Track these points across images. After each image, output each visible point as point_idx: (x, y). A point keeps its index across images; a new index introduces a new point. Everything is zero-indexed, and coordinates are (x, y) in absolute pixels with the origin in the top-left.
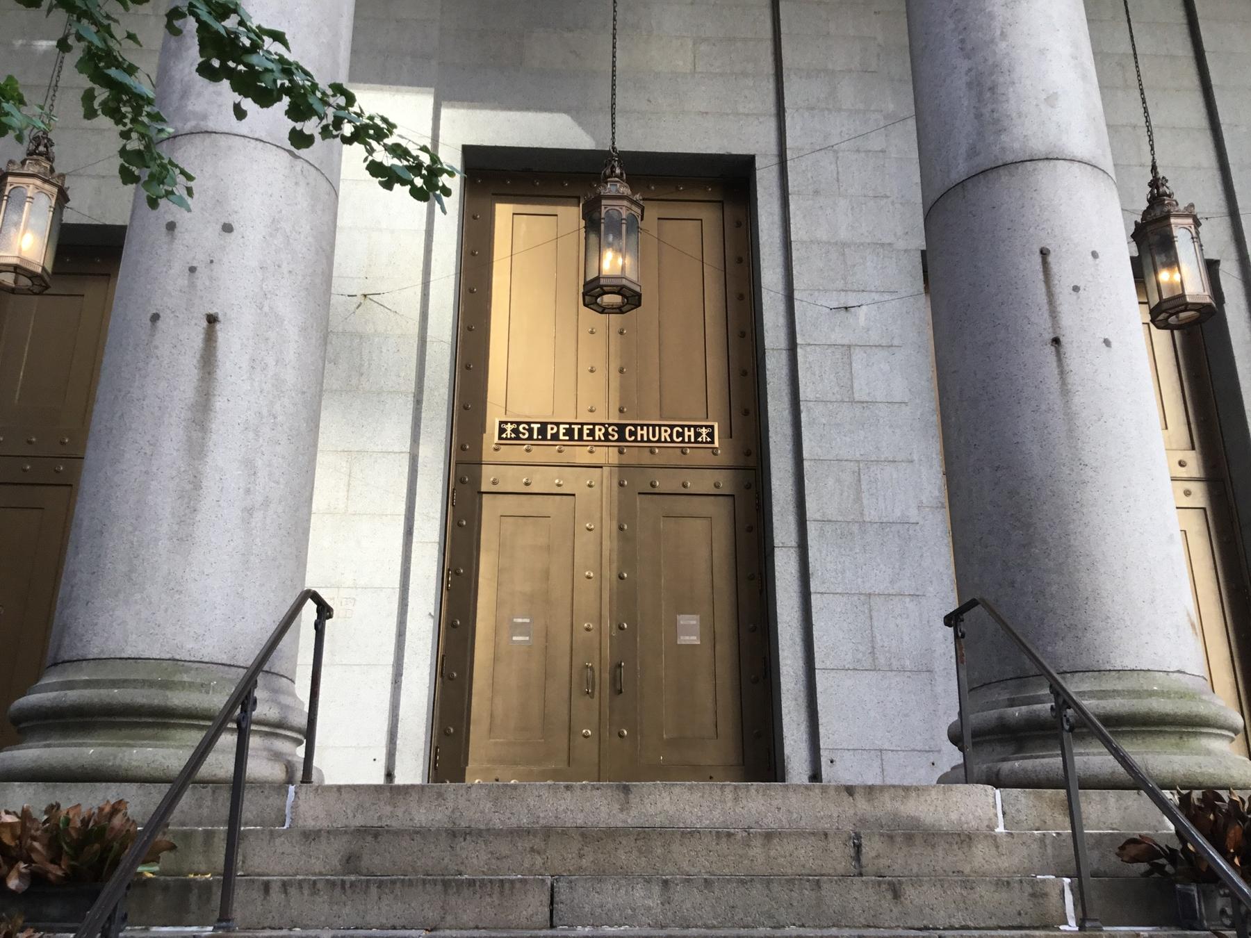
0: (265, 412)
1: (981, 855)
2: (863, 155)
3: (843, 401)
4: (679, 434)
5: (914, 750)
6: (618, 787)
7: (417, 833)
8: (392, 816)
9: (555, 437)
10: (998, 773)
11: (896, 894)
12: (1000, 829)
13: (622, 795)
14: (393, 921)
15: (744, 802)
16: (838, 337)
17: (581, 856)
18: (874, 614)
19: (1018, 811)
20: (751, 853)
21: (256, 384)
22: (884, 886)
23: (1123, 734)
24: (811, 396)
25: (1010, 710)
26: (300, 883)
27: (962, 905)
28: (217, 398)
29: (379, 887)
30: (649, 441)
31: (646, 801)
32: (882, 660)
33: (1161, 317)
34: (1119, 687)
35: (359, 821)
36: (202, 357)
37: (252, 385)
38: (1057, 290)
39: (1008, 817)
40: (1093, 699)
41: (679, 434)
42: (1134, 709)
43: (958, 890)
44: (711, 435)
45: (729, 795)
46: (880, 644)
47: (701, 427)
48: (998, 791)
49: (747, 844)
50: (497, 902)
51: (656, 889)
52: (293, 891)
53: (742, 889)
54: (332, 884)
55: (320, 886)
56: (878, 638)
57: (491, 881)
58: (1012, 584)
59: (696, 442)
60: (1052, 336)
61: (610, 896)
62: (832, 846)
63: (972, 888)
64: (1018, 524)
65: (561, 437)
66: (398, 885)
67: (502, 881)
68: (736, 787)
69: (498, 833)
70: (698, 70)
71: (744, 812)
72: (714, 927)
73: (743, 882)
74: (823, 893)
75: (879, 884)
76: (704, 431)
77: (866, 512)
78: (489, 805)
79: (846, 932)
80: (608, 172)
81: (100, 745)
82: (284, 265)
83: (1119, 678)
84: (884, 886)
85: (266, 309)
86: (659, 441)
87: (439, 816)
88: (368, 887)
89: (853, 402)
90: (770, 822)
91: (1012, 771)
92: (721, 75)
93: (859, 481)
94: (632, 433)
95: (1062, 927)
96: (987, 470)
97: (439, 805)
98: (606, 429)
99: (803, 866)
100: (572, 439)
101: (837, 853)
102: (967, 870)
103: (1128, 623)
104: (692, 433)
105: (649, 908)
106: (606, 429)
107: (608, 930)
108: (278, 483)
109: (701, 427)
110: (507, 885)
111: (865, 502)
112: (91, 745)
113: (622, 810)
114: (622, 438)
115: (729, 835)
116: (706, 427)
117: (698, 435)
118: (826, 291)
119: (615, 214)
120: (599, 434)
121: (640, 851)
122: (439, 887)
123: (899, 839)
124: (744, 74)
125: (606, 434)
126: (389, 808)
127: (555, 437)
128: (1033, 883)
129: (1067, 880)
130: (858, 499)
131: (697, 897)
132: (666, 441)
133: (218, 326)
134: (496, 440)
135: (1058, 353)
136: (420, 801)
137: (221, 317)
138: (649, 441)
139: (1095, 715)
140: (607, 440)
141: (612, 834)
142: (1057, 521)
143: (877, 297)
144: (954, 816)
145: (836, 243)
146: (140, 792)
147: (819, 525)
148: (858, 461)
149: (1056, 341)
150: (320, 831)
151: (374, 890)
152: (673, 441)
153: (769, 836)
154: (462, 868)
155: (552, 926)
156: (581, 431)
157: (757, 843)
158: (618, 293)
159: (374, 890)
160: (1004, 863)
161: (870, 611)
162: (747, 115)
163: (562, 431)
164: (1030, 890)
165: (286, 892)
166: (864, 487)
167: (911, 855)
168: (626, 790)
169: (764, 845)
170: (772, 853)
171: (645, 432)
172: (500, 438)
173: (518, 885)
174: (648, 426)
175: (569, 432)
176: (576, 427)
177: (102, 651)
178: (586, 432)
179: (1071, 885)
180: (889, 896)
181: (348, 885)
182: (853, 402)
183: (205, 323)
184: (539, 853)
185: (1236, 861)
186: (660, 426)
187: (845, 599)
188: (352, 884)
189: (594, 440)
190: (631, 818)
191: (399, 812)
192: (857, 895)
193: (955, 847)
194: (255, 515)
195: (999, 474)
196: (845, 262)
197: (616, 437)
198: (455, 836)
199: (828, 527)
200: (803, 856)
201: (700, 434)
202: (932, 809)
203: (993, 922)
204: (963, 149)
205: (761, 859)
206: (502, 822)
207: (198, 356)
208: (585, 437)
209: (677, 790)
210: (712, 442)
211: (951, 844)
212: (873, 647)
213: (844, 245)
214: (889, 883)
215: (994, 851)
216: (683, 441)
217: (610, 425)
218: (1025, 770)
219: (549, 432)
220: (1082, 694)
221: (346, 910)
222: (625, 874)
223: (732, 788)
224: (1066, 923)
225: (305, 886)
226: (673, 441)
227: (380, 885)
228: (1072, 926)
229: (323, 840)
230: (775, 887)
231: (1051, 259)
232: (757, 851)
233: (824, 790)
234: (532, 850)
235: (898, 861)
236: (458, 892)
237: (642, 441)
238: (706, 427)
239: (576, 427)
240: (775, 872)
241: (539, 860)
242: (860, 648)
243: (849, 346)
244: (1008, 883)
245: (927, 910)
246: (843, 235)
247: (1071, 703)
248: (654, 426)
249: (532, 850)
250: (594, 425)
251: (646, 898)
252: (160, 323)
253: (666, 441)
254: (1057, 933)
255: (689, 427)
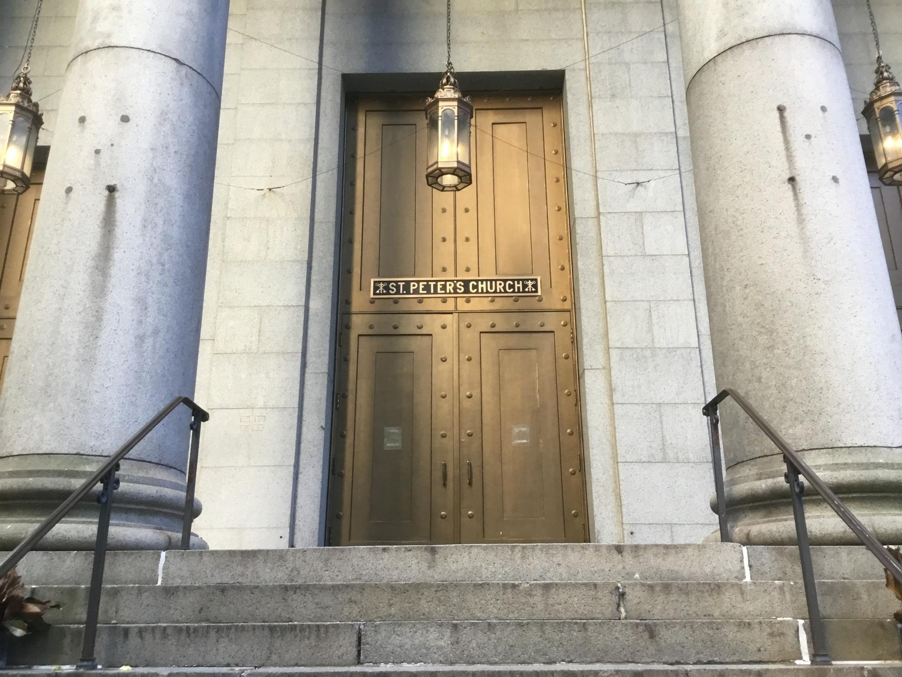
0: (154, 260)
1: (728, 601)
2: (649, 66)
3: (636, 255)
4: (510, 286)
5: (697, 524)
6: (426, 549)
7: (257, 587)
8: (242, 575)
9: (416, 291)
10: (748, 535)
11: (652, 636)
12: (748, 579)
13: (429, 554)
14: (229, 660)
15: (531, 559)
16: (632, 206)
17: (390, 605)
18: (664, 418)
19: (763, 564)
20: (531, 601)
21: (148, 239)
22: (641, 628)
23: (853, 499)
24: (611, 253)
25: (758, 483)
26: (153, 629)
27: (709, 643)
28: (116, 250)
29: (217, 632)
30: (487, 292)
31: (449, 560)
32: (671, 455)
33: (887, 175)
34: (850, 461)
35: (217, 580)
36: (104, 219)
37: (144, 240)
38: (792, 139)
39: (754, 569)
40: (823, 469)
41: (510, 286)
42: (862, 478)
43: (706, 630)
44: (535, 286)
45: (518, 555)
46: (669, 442)
47: (528, 280)
48: (744, 549)
49: (529, 593)
50: (314, 644)
51: (448, 633)
52: (148, 636)
53: (520, 631)
54: (179, 630)
55: (169, 631)
56: (668, 437)
57: (309, 626)
58: (759, 380)
59: (524, 292)
60: (788, 176)
61: (408, 638)
62: (600, 594)
63: (717, 629)
64: (763, 330)
65: (421, 291)
66: (233, 630)
67: (318, 626)
68: (524, 548)
69: (323, 588)
70: (521, 7)
71: (531, 567)
72: (496, 663)
73: (520, 625)
74: (589, 634)
75: (637, 625)
76: (530, 283)
77: (656, 340)
78: (321, 565)
79: (164, 671)
80: (444, 81)
81: (16, 522)
82: (171, 146)
83: (850, 453)
84: (641, 628)
85: (156, 181)
86: (495, 292)
87: (280, 575)
88: (208, 632)
89: (644, 255)
90: (551, 578)
91: (760, 532)
92: (538, 11)
93: (650, 316)
94: (475, 287)
95: (798, 662)
96: (738, 288)
97: (281, 566)
98: (455, 284)
99: (576, 612)
100: (429, 292)
101: (605, 601)
102: (717, 614)
103: (857, 408)
104: (520, 285)
105: (440, 648)
106: (455, 284)
107: (407, 667)
108: (166, 316)
109: (528, 280)
110: (322, 630)
111: (655, 333)
112: (10, 522)
113: (429, 567)
114: (467, 291)
115: (514, 586)
116: (532, 280)
117: (525, 286)
118: (622, 171)
119: (448, 112)
120: (449, 288)
121: (439, 600)
122: (267, 632)
123: (658, 589)
124: (556, 9)
125: (455, 288)
126: (240, 569)
127: (416, 291)
128: (771, 625)
129: (801, 622)
130: (650, 329)
131: (481, 637)
132: (501, 292)
133: (117, 194)
134: (372, 296)
135: (794, 189)
136: (265, 562)
137: (119, 187)
138: (487, 292)
139: (830, 488)
140: (455, 292)
141: (418, 587)
142: (795, 326)
143: (662, 174)
144: (708, 570)
145: (629, 134)
146: (45, 558)
147: (618, 352)
148: (649, 301)
149: (792, 180)
150: (178, 587)
151: (213, 634)
152: (506, 292)
153: (547, 587)
154: (293, 616)
155: (359, 663)
156: (435, 287)
157: (539, 592)
158: (453, 174)
159: (213, 634)
160: (750, 607)
161: (661, 416)
162: (559, 40)
163: (421, 287)
164: (769, 630)
165: (142, 637)
166: (655, 320)
167: (668, 603)
168: (433, 551)
169: (543, 595)
170: (550, 602)
171: (484, 285)
172: (375, 294)
173: (331, 630)
174: (487, 281)
175: (427, 288)
176: (432, 284)
177: (24, 449)
178: (439, 287)
179: (804, 625)
180: (646, 635)
181: (192, 630)
182: (644, 255)
183: (106, 193)
184: (355, 602)
185: (10, 185)
186: (496, 281)
187: (641, 408)
188: (196, 630)
189: (446, 293)
190: (437, 575)
191: (249, 572)
192: (617, 635)
193: (706, 594)
194: (147, 341)
195: (747, 291)
196: (637, 149)
197: (463, 289)
198: (287, 590)
199: (627, 353)
200: (577, 604)
201: (527, 286)
202: (689, 563)
203: (735, 658)
204: (714, 33)
205: (540, 606)
206: (332, 579)
207: (101, 218)
208: (439, 291)
209: (475, 551)
210: (536, 291)
211: (703, 592)
212: (664, 445)
213: (636, 135)
214: (646, 625)
215: (739, 598)
216: (514, 292)
217: (458, 281)
218: (770, 531)
219: (412, 288)
220: (818, 467)
221: (191, 651)
222: (427, 619)
223: (519, 548)
224: (801, 658)
225: (157, 631)
226: (506, 292)
227: (219, 630)
228: (806, 660)
229: (181, 594)
230: (548, 630)
231: (786, 114)
232: (537, 598)
233: (597, 549)
234: (350, 601)
235: (659, 608)
236: (282, 635)
237: (482, 292)
238: (532, 280)
239: (432, 284)
240: (552, 616)
241: (356, 610)
242: (654, 445)
243: (641, 213)
244: (749, 624)
245: (679, 648)
246: (635, 128)
247: (801, 470)
248: (491, 281)
249: (350, 601)
250: (446, 281)
251: (438, 639)
252: (73, 195)
253: (501, 292)
254: (792, 667)
255: (518, 281)
